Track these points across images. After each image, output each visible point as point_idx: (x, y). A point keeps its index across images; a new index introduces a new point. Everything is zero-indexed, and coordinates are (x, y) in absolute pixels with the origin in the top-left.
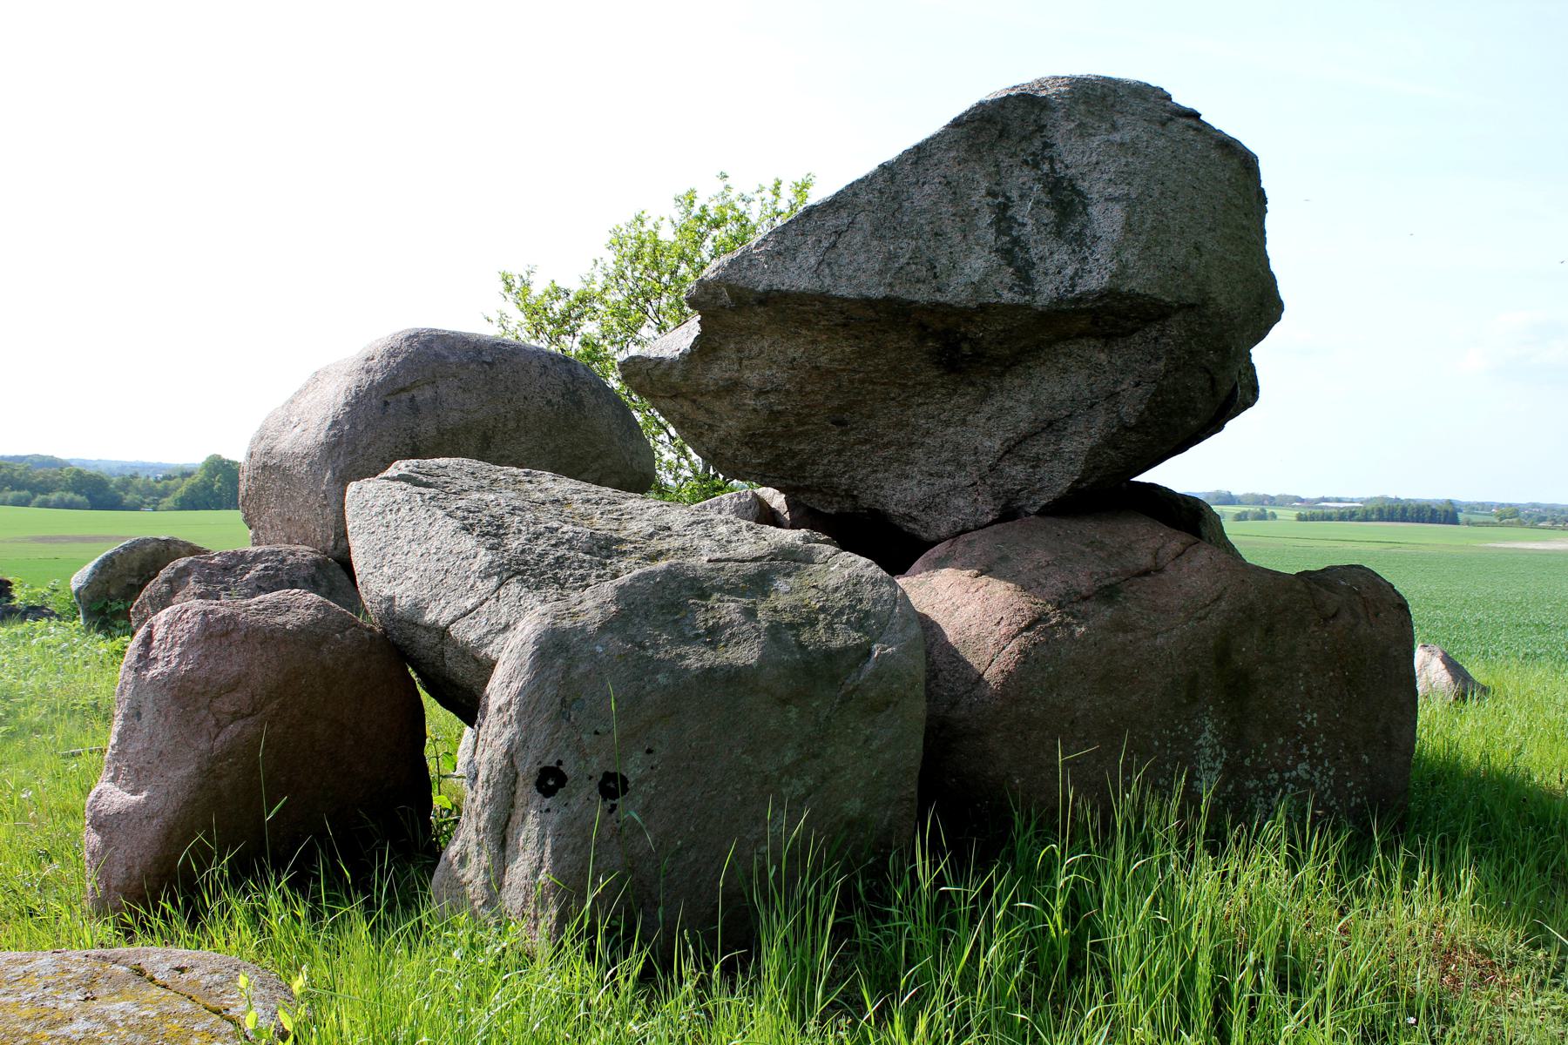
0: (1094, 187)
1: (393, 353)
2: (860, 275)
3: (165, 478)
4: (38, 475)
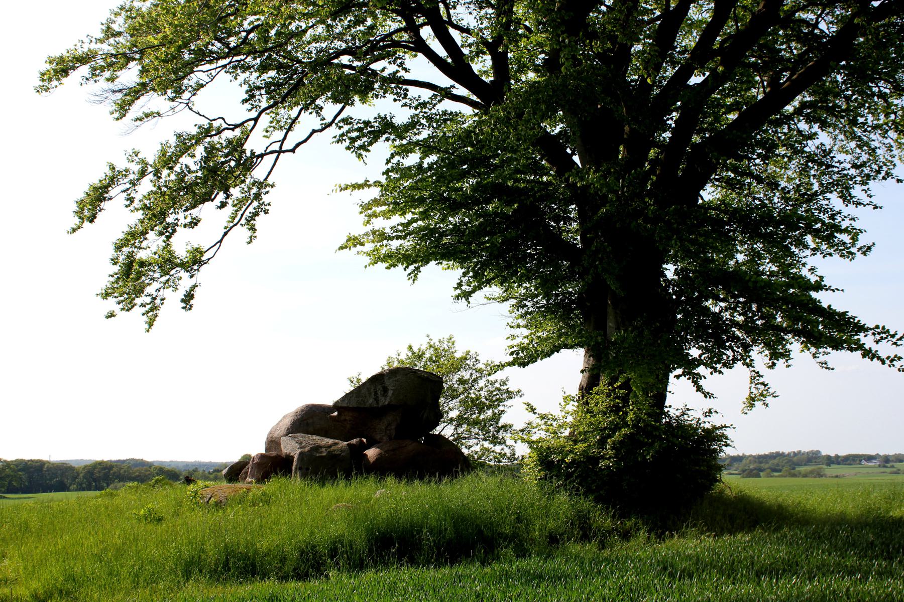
0: (390, 388)
1: (302, 411)
2: (353, 404)
3: (214, 471)
4: (136, 471)
